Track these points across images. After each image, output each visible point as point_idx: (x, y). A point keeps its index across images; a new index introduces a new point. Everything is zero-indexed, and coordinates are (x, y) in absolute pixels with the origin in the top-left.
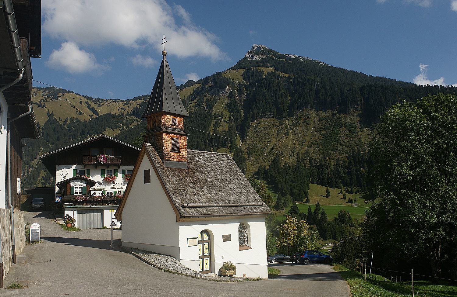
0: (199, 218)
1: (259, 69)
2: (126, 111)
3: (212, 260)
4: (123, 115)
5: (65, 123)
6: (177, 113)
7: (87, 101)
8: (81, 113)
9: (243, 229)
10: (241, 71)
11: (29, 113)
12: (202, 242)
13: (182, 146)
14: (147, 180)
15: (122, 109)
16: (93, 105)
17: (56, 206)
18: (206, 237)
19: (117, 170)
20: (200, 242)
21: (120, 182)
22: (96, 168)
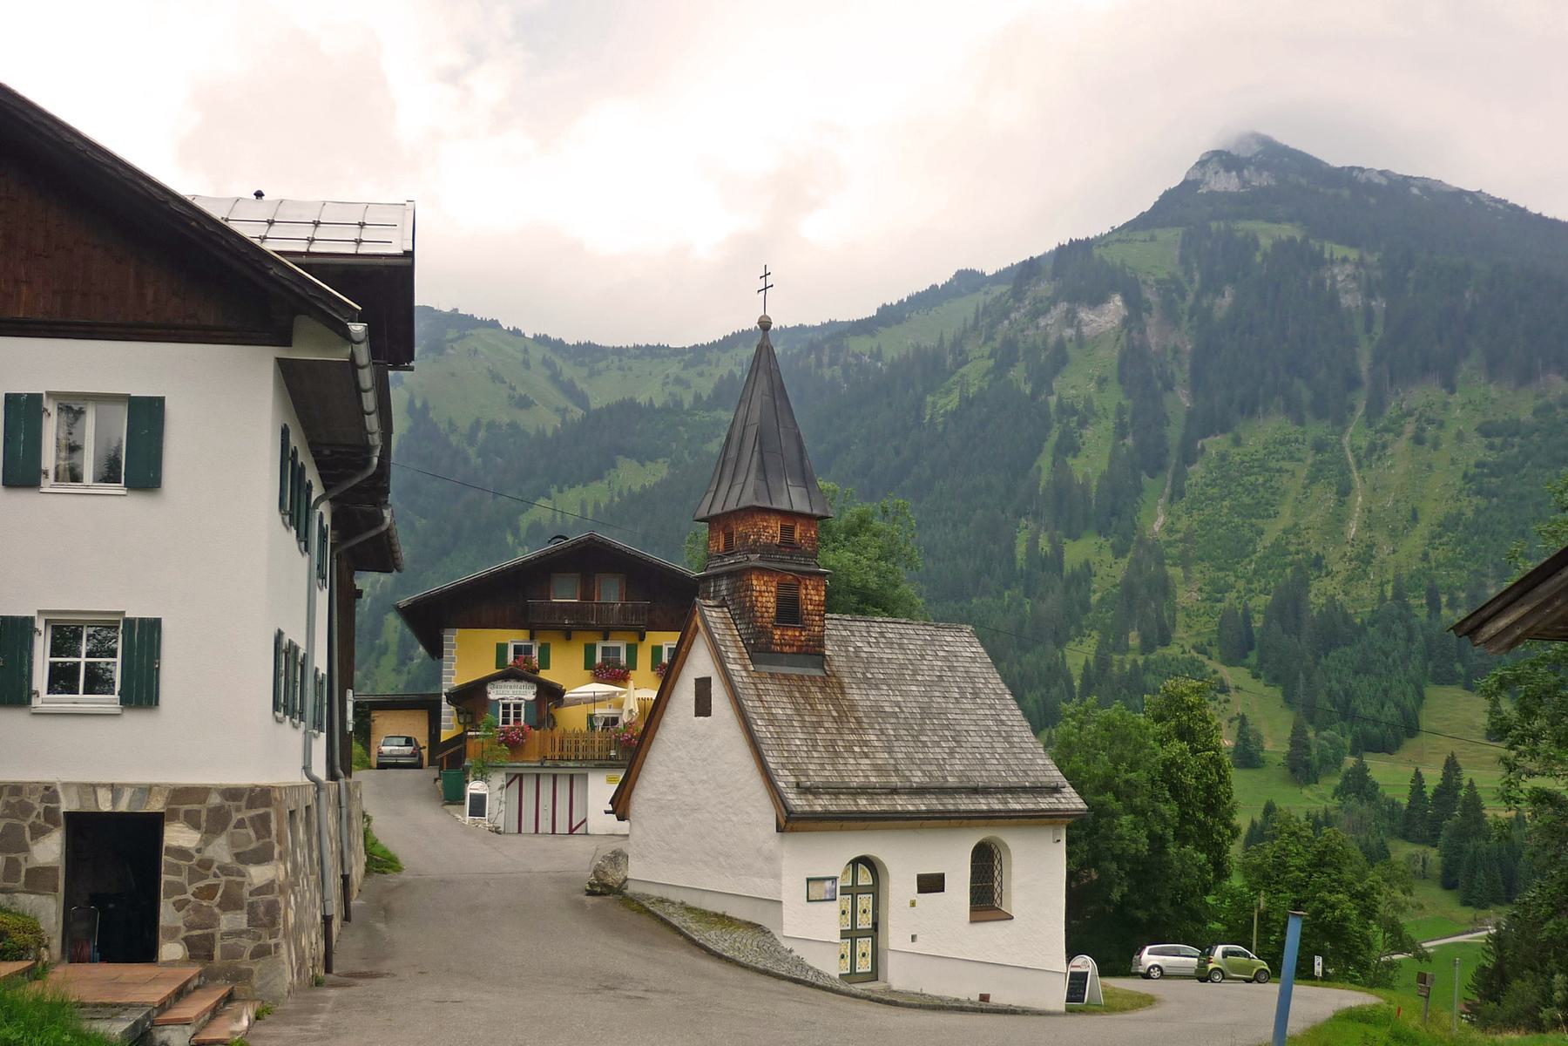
1: (1244, 226)
2: (693, 390)
4: (679, 404)
5: (471, 438)
6: (795, 509)
7: (548, 355)
8: (524, 403)
9: (985, 863)
10: (1173, 235)
11: (383, 528)
12: (853, 891)
13: (809, 607)
15: (679, 381)
16: (568, 371)
17: (442, 759)
18: (865, 878)
19: (636, 645)
20: (844, 890)
21: (639, 691)
22: (568, 638)
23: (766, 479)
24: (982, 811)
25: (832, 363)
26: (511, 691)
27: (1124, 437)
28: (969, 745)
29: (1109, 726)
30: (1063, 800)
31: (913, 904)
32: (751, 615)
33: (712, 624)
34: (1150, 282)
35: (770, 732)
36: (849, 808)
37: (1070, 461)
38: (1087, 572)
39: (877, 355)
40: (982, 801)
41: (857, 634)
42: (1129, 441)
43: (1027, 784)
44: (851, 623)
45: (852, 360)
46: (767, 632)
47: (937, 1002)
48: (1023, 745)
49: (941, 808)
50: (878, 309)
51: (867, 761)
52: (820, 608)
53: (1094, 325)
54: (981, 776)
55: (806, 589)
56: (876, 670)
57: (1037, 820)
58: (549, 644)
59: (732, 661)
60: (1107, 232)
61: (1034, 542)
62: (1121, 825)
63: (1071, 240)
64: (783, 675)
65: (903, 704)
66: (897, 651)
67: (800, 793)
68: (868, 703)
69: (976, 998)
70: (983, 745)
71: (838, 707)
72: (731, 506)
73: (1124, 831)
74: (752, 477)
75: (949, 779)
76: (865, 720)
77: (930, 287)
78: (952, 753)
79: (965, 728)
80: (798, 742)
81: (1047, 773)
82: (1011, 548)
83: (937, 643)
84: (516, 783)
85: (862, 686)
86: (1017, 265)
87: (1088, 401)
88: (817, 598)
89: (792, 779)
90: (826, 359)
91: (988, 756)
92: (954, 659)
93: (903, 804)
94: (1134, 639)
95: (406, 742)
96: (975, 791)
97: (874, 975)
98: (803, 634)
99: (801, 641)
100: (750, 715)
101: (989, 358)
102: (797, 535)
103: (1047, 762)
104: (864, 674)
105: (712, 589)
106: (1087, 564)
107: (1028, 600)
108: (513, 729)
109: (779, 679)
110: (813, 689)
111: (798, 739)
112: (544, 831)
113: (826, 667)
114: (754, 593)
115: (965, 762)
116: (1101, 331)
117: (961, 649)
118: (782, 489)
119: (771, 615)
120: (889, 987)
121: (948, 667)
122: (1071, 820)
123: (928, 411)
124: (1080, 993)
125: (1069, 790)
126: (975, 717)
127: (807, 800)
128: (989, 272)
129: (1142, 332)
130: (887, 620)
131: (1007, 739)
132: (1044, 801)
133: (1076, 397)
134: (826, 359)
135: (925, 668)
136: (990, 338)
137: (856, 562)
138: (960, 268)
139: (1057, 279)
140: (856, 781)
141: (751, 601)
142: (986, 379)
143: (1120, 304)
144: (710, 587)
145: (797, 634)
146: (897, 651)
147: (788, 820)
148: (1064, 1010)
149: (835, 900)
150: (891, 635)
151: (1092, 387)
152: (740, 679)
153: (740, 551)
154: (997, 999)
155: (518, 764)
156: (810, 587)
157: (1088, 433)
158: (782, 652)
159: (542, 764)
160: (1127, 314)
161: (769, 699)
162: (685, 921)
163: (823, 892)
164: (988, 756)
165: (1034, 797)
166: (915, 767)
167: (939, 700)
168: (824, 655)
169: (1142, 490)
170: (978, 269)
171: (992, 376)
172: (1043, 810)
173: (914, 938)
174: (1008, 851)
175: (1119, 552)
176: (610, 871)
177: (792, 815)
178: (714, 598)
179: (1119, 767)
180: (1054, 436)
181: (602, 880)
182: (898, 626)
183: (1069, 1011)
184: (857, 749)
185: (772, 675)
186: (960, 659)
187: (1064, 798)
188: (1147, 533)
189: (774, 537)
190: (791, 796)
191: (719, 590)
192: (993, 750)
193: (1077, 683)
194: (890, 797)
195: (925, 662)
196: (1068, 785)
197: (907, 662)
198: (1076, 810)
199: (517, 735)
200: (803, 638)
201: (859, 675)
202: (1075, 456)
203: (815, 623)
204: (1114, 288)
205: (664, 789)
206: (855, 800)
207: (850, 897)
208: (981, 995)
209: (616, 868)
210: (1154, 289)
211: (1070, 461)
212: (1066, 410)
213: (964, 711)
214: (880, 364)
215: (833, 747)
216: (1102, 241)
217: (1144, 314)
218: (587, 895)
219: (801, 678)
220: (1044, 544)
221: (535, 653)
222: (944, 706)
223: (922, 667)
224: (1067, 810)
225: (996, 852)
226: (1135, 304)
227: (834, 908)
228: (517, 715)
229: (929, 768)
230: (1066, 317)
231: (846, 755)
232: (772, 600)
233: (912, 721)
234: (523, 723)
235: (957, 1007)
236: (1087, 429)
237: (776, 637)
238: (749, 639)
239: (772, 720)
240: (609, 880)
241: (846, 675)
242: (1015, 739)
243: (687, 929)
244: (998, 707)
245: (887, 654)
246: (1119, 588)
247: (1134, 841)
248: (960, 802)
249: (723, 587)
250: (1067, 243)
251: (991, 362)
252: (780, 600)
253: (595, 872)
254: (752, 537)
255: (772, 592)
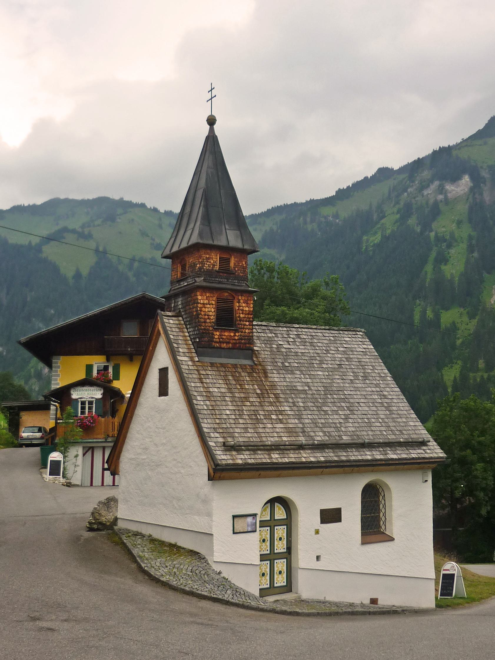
0: (260, 472)
3: (293, 565)
13: (242, 316)
14: (163, 391)
18: (280, 513)
20: (263, 524)
23: (209, 225)
24: (368, 461)
25: (312, 221)
26: (86, 393)
27: (472, 252)
28: (359, 412)
29: (466, 409)
30: (428, 451)
31: (317, 532)
32: (197, 320)
33: (168, 328)
34: (485, 167)
35: (206, 405)
36: (264, 461)
37: (443, 267)
38: (454, 328)
39: (336, 216)
40: (368, 453)
41: (279, 335)
42: (476, 254)
43: (402, 440)
44: (276, 329)
45: (323, 219)
46: (209, 333)
47: (334, 609)
48: (400, 412)
49: (336, 459)
50: (336, 192)
51: (281, 426)
52: (250, 316)
53: (454, 192)
54: (368, 435)
55: (239, 302)
56: (292, 361)
57: (393, 467)
58: (120, 364)
59: (181, 354)
60: (460, 142)
61: (424, 313)
62: (477, 470)
63: (440, 147)
64: (221, 364)
65: (311, 384)
66: (309, 348)
67: (226, 450)
68: (285, 384)
69: (367, 602)
70: (370, 412)
71: (261, 386)
72: (184, 245)
73: (478, 473)
74: (198, 223)
75: (344, 437)
76: (281, 396)
77: (364, 178)
78: (347, 418)
79: (357, 401)
80: (228, 412)
81: (416, 432)
82: (411, 317)
83: (339, 342)
84: (89, 454)
85: (281, 372)
86: (411, 163)
87: (452, 234)
88: (247, 309)
89: (221, 440)
90: (308, 220)
91: (373, 420)
92: (351, 353)
93: (307, 456)
94: (481, 364)
95: (39, 430)
96: (363, 446)
97: (288, 588)
98: (237, 334)
99: (235, 339)
100: (191, 393)
101: (397, 214)
102: (232, 264)
103: (417, 424)
104: (282, 363)
105: (173, 305)
106: (454, 323)
107: (422, 345)
108: (87, 417)
109: (217, 367)
110: (243, 374)
111: (228, 410)
112: (108, 484)
113: (255, 359)
114: (199, 305)
115: (356, 425)
116: (458, 195)
117: (356, 346)
118: (222, 231)
119: (212, 321)
120: (299, 597)
121: (346, 358)
122: (434, 466)
123: (364, 245)
124: (451, 590)
125: (433, 444)
126: (365, 393)
127: (232, 455)
128: (396, 168)
129: (481, 194)
130: (303, 326)
131: (388, 408)
132: (414, 452)
133: (445, 232)
134: (308, 220)
135: (329, 359)
136: (397, 203)
137: (312, 314)
138: (380, 167)
139: (433, 169)
140: (270, 441)
141: (197, 311)
142: (396, 225)
143: (468, 180)
144: (171, 304)
145: (232, 334)
146: (309, 348)
147: (215, 470)
148: (435, 606)
149: (255, 531)
150: (305, 337)
151: (454, 226)
152: (186, 367)
153: (190, 276)
154: (385, 601)
155: (90, 440)
156: (242, 301)
157: (452, 251)
158: (221, 348)
159: (106, 440)
160: (472, 185)
161: (208, 381)
162: (143, 551)
163: (246, 525)
164: (373, 420)
165: (407, 449)
166: (318, 429)
167: (338, 381)
168: (253, 350)
169: (484, 281)
170: (390, 167)
171: (399, 223)
172: (413, 458)
173: (318, 558)
174: (389, 489)
175: (472, 316)
176: (103, 513)
177: (218, 467)
178: (174, 311)
179: (474, 434)
180: (433, 255)
181: (98, 519)
182: (311, 330)
183: (439, 606)
184: (274, 417)
185: (212, 365)
186: (355, 353)
187: (429, 449)
188: (487, 305)
189: (215, 265)
190: (219, 453)
191: (177, 305)
192: (377, 416)
193: (450, 390)
194: (297, 452)
195: (329, 355)
196: (431, 440)
197: (316, 355)
198: (438, 458)
199: (89, 421)
200: (236, 338)
201: (279, 364)
202: (445, 264)
203: (245, 327)
204: (464, 172)
205: (140, 451)
206: (269, 455)
207: (269, 528)
208: (371, 599)
209: (108, 511)
210: (487, 171)
211: (443, 267)
212: (439, 239)
213: (357, 389)
214: (337, 221)
215: (256, 415)
216: (458, 146)
217: (482, 185)
218: (88, 531)
219: (235, 366)
220: (430, 314)
221: (111, 370)
222: (342, 385)
223: (326, 359)
224: (431, 458)
225: (380, 490)
226: (476, 179)
227: (255, 537)
228: (90, 408)
229: (329, 430)
230: (439, 188)
231: (265, 421)
232: (213, 310)
233: (317, 396)
234: (94, 413)
235: (349, 612)
236: (452, 249)
237: (216, 337)
238: (195, 338)
239: (209, 396)
240: (103, 519)
241: (269, 364)
242: (394, 408)
243: (140, 557)
244: (382, 386)
245: (301, 349)
246: (472, 336)
247: (485, 479)
248: (351, 454)
249: (180, 303)
250: (438, 149)
251: (398, 216)
252: (218, 310)
253: (93, 514)
254: (198, 265)
255: (213, 304)
